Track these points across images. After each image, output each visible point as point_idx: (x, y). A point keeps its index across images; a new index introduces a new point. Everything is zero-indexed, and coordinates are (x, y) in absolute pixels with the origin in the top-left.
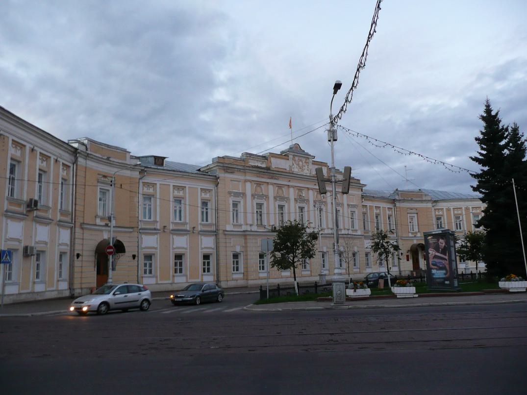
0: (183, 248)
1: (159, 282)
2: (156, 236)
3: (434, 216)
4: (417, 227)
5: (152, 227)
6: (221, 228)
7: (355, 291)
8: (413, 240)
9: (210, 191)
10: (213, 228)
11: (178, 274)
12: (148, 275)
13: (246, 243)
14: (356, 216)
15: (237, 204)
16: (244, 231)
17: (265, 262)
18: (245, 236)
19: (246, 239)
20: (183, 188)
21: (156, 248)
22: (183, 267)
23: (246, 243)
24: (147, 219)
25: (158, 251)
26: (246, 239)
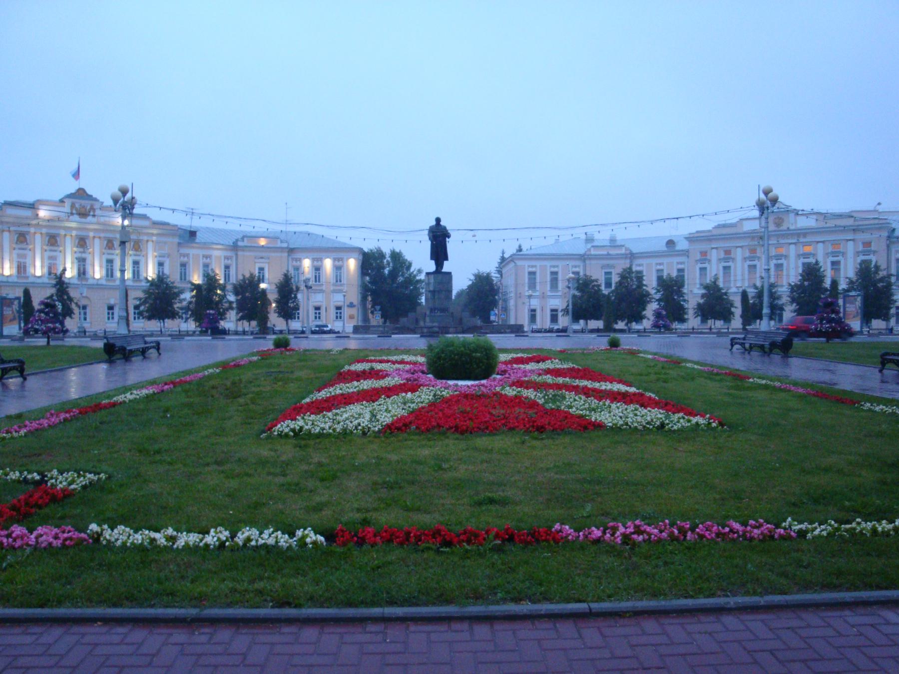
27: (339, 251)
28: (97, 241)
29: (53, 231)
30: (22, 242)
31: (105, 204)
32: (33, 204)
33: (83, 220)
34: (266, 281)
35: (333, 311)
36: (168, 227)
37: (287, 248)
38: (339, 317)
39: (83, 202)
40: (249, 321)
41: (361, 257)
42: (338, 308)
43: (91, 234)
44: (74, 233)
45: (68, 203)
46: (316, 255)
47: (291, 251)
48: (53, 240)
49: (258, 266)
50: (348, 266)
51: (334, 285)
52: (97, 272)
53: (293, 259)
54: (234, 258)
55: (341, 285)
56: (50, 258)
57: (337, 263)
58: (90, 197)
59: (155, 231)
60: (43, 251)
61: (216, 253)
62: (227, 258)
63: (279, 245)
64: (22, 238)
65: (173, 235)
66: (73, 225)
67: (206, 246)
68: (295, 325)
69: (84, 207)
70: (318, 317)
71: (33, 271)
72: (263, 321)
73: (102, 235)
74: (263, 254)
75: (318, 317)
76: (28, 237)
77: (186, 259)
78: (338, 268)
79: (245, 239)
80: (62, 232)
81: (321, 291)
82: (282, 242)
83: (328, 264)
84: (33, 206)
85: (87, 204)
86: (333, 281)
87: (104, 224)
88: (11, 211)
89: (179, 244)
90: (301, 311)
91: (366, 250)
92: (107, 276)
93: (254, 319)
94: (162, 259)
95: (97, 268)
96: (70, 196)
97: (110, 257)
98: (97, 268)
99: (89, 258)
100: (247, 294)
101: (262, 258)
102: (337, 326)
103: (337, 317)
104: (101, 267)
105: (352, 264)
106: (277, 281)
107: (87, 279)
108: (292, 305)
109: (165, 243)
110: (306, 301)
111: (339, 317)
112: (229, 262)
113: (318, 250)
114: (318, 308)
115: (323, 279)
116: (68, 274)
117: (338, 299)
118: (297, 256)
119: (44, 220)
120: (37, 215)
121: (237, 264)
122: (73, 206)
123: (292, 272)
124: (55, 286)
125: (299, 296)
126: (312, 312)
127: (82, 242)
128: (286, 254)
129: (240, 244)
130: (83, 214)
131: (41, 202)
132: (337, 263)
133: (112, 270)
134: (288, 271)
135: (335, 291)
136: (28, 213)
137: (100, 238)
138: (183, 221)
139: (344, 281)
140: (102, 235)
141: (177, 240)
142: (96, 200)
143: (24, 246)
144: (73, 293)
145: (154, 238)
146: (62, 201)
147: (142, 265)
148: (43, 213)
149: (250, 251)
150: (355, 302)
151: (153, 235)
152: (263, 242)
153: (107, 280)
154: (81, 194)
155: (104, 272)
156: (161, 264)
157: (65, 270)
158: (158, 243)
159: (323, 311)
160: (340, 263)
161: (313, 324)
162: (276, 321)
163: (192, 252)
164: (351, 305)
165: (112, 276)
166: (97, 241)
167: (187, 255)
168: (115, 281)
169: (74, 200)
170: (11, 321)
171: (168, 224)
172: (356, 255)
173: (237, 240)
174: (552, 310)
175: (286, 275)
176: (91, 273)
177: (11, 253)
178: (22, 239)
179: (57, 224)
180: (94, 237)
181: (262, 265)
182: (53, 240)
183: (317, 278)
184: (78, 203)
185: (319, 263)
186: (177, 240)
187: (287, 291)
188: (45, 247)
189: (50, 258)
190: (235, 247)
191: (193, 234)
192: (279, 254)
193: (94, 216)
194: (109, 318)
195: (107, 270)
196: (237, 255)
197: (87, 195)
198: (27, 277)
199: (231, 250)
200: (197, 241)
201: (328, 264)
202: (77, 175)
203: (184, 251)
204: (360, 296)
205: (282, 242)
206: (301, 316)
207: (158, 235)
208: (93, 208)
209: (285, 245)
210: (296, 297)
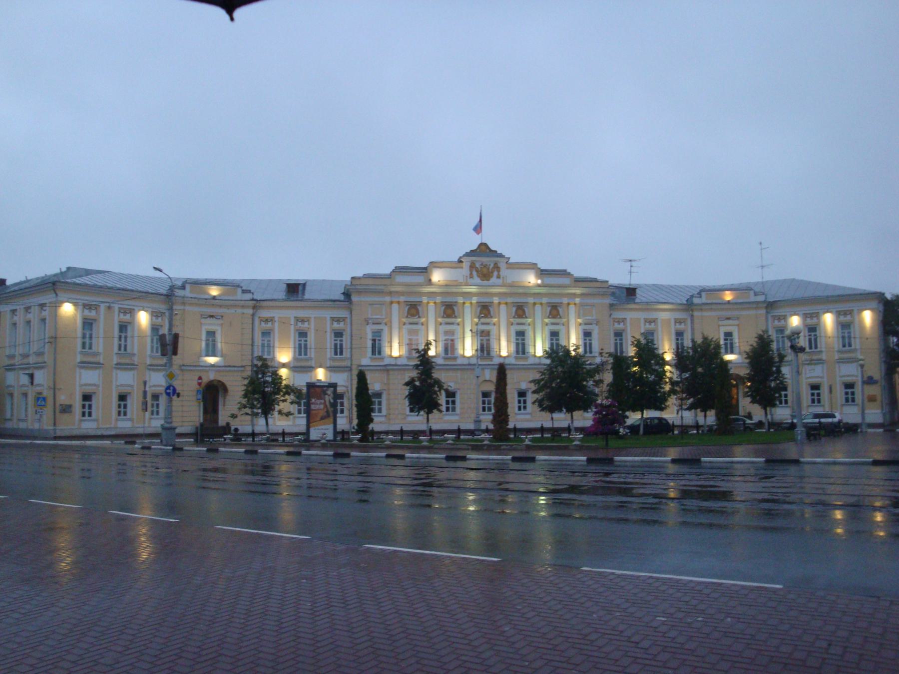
0: (95, 385)
1: (101, 426)
2: (97, 371)
3: (328, 330)
4: (349, 350)
5: (128, 361)
6: (354, 362)
7: (213, 450)
8: (207, 371)
9: (344, 319)
10: (348, 363)
11: (122, 417)
12: (87, 418)
13: (388, 379)
14: (100, 329)
15: (126, 327)
16: (386, 366)
17: (94, 408)
18: (388, 370)
19: (388, 375)
20: (308, 320)
21: (132, 386)
22: (821, 397)
23: (388, 379)
24: (303, 357)
25: (100, 389)
26: (388, 375)
27: (845, 301)
28: (503, 307)
29: (449, 299)
30: (413, 316)
31: (511, 261)
32: (425, 269)
33: (486, 283)
34: (736, 350)
35: (839, 392)
36: (598, 285)
37: (764, 302)
38: (850, 399)
39: (485, 260)
40: (704, 410)
41: (881, 308)
42: (849, 386)
43: (496, 300)
44: (475, 300)
45: (466, 265)
46: (810, 309)
47: (770, 306)
48: (449, 310)
49: (723, 330)
50: (861, 322)
51: (839, 351)
52: (468, 348)
53: (774, 317)
54: (348, 320)
55: (307, 360)
56: (446, 333)
57: (842, 318)
58: (494, 253)
59: (578, 291)
60: (438, 324)
61: (664, 316)
62: (678, 321)
63: (753, 298)
64: (414, 310)
65: (604, 295)
66: (473, 289)
67: (648, 306)
68: (782, 413)
69: (485, 266)
70: (816, 400)
71: (461, 352)
72: (727, 410)
73: (510, 300)
74: (736, 313)
75: (816, 400)
76: (420, 308)
77: (621, 326)
78: (845, 327)
79: (703, 294)
80: (460, 300)
81: (820, 361)
82: (756, 294)
83: (828, 320)
84: (424, 271)
85: (488, 261)
86: (837, 345)
87: (511, 286)
88: (400, 278)
89: (611, 306)
90: (789, 392)
91: (889, 296)
92: (517, 352)
93: (711, 407)
94: (588, 327)
95: (504, 343)
96: (472, 253)
97: (520, 328)
98: (504, 343)
99: (493, 330)
100: (700, 370)
101: (728, 319)
102: (849, 414)
103: (847, 400)
104: (508, 341)
105: (868, 317)
106: (748, 349)
107: (491, 358)
108: (773, 384)
109: (593, 305)
110: (797, 376)
111: (850, 399)
112: (681, 327)
113: (814, 300)
114: (815, 387)
115: (822, 345)
116: (432, 353)
117: (851, 372)
118: (777, 312)
119: (440, 286)
120: (430, 280)
121: (693, 329)
122: (472, 266)
123: (773, 334)
124: (416, 367)
125: (785, 370)
126: (806, 395)
127: (485, 310)
128: (763, 311)
129: (696, 301)
130: (485, 275)
131: (434, 265)
132: (809, 321)
133: (523, 345)
134: (766, 331)
135: (841, 361)
136: (420, 279)
137: (398, 302)
138: (619, 278)
139: (856, 344)
140: (510, 300)
141: (608, 301)
142: (501, 256)
143: (415, 320)
144: (436, 375)
145: (577, 300)
146: (460, 261)
147: (562, 336)
148: (437, 277)
149: (711, 310)
150: (877, 376)
151: (575, 295)
152: (728, 296)
153: (516, 358)
154: (484, 250)
155: (513, 348)
156: (587, 334)
157: (428, 344)
158: (582, 305)
159: (825, 391)
160: (848, 318)
161: (809, 414)
162: (748, 407)
163: (629, 315)
164: (870, 381)
165: (524, 353)
166: (503, 307)
167: (624, 320)
168: (527, 358)
169: (474, 258)
170: (322, 418)
171: (595, 280)
172: (874, 304)
173: (692, 296)
174: (454, 409)
175: (761, 338)
176: (531, 350)
177: (400, 328)
178: (413, 311)
179: (454, 290)
180: (500, 303)
181: (211, 328)
182: (449, 310)
183: (813, 343)
184: (479, 260)
185: (815, 320)
186: (608, 301)
187: (764, 360)
188: (440, 320)
189: (446, 333)
190: (689, 306)
191: (631, 292)
192: (752, 312)
193: (498, 277)
194: (520, 409)
195: (517, 344)
196: (171, 309)
197: (491, 250)
198: (455, 358)
199: (686, 310)
200: (637, 301)
201: (828, 320)
202: (478, 229)
203: (618, 315)
204: (883, 367)
205: (756, 294)
206: (789, 398)
207: (582, 294)
208: (497, 267)
209: (761, 298)
210: (779, 371)
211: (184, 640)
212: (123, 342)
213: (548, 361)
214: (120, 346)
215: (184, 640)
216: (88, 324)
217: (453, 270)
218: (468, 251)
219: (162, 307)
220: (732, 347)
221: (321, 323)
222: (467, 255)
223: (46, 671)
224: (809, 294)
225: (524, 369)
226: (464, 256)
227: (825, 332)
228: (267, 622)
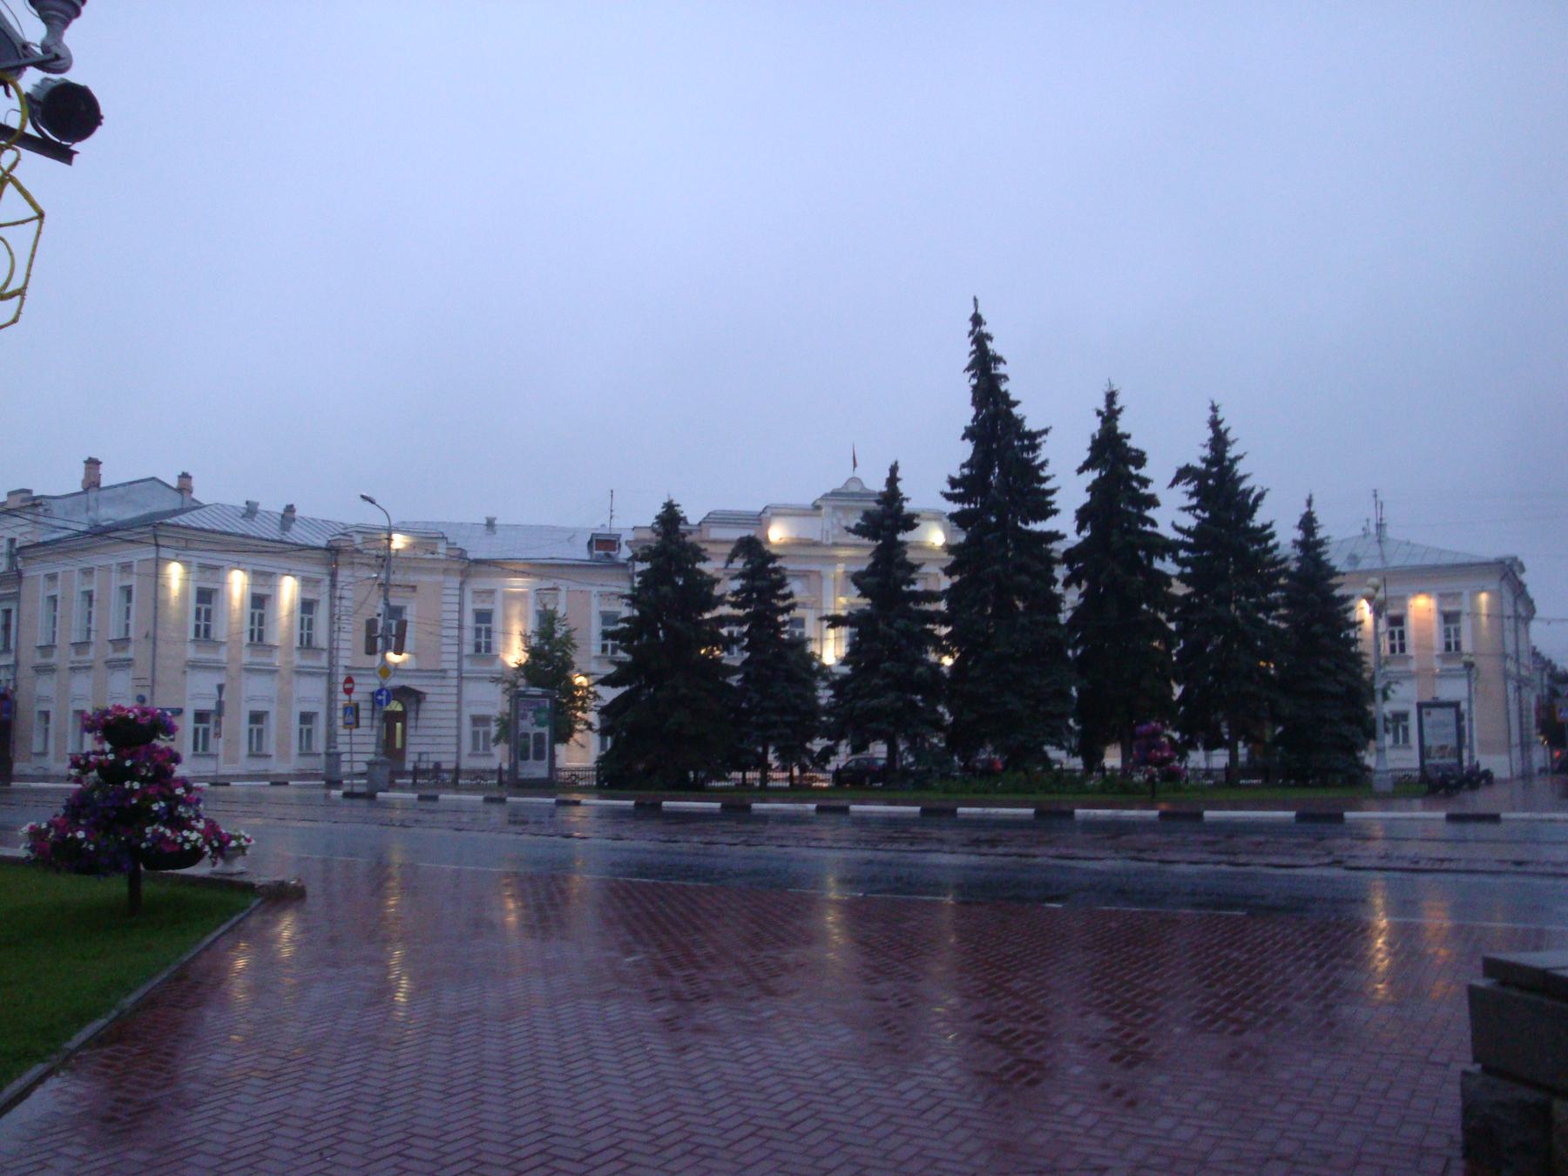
46: (265, 563)
146: (817, 507)
196: (333, 575)
211: (266, 1136)
212: (202, 624)
213: (846, 670)
214: (198, 627)
215: (266, 1136)
216: (1449, 618)
217: (802, 519)
218: (829, 490)
219: (319, 572)
220: (401, 637)
221: (359, 592)
222: (826, 497)
223: (320, 1172)
224: (1430, 560)
225: (310, 674)
226: (822, 499)
227: (230, 604)
228: (420, 1111)
